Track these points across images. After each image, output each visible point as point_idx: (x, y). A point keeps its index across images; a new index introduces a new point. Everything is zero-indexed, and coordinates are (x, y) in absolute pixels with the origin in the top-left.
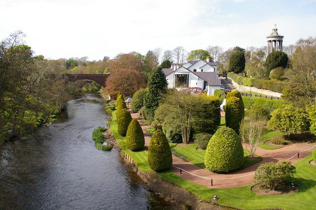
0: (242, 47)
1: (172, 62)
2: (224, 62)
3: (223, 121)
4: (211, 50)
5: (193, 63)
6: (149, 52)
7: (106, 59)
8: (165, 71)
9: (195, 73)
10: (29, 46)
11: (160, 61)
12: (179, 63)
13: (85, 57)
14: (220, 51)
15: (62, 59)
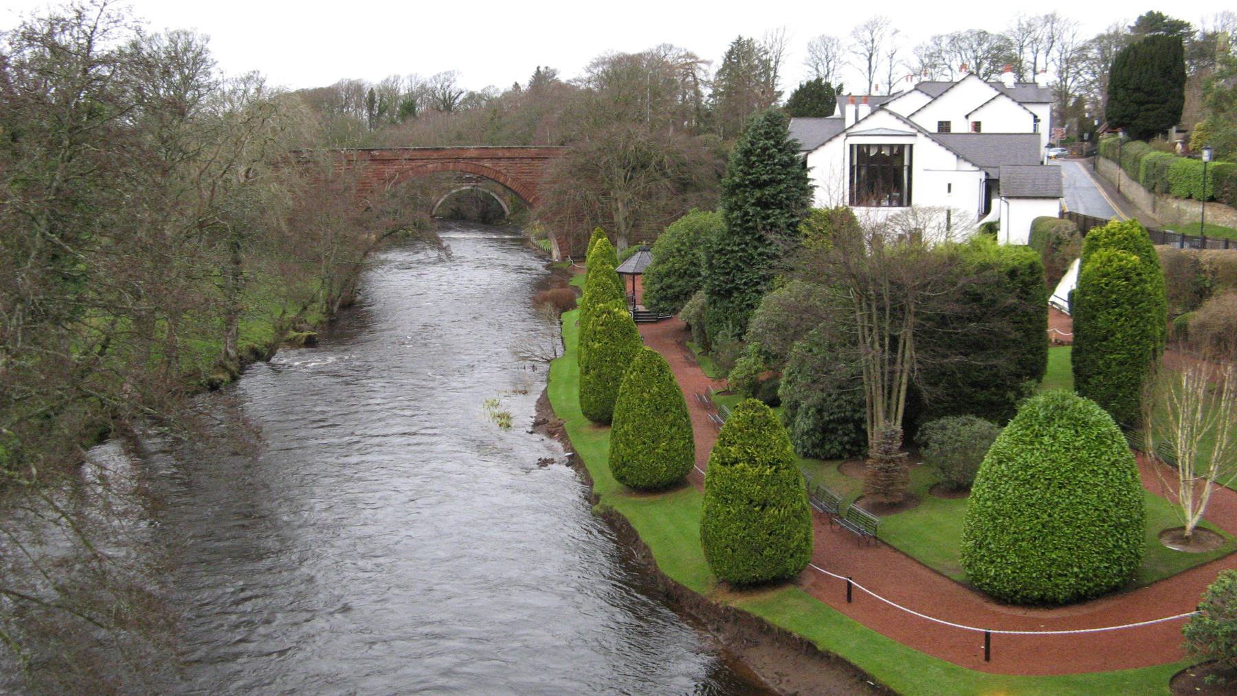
0: (1173, 13)
1: (840, 88)
2: (1087, 88)
3: (1059, 359)
4: (1027, 30)
5: (935, 90)
6: (739, 42)
7: (542, 80)
8: (799, 129)
9: (943, 137)
10: (1186, 22)
11: (788, 82)
12: (874, 93)
13: (452, 74)
14: (1067, 37)
15: (351, 83)
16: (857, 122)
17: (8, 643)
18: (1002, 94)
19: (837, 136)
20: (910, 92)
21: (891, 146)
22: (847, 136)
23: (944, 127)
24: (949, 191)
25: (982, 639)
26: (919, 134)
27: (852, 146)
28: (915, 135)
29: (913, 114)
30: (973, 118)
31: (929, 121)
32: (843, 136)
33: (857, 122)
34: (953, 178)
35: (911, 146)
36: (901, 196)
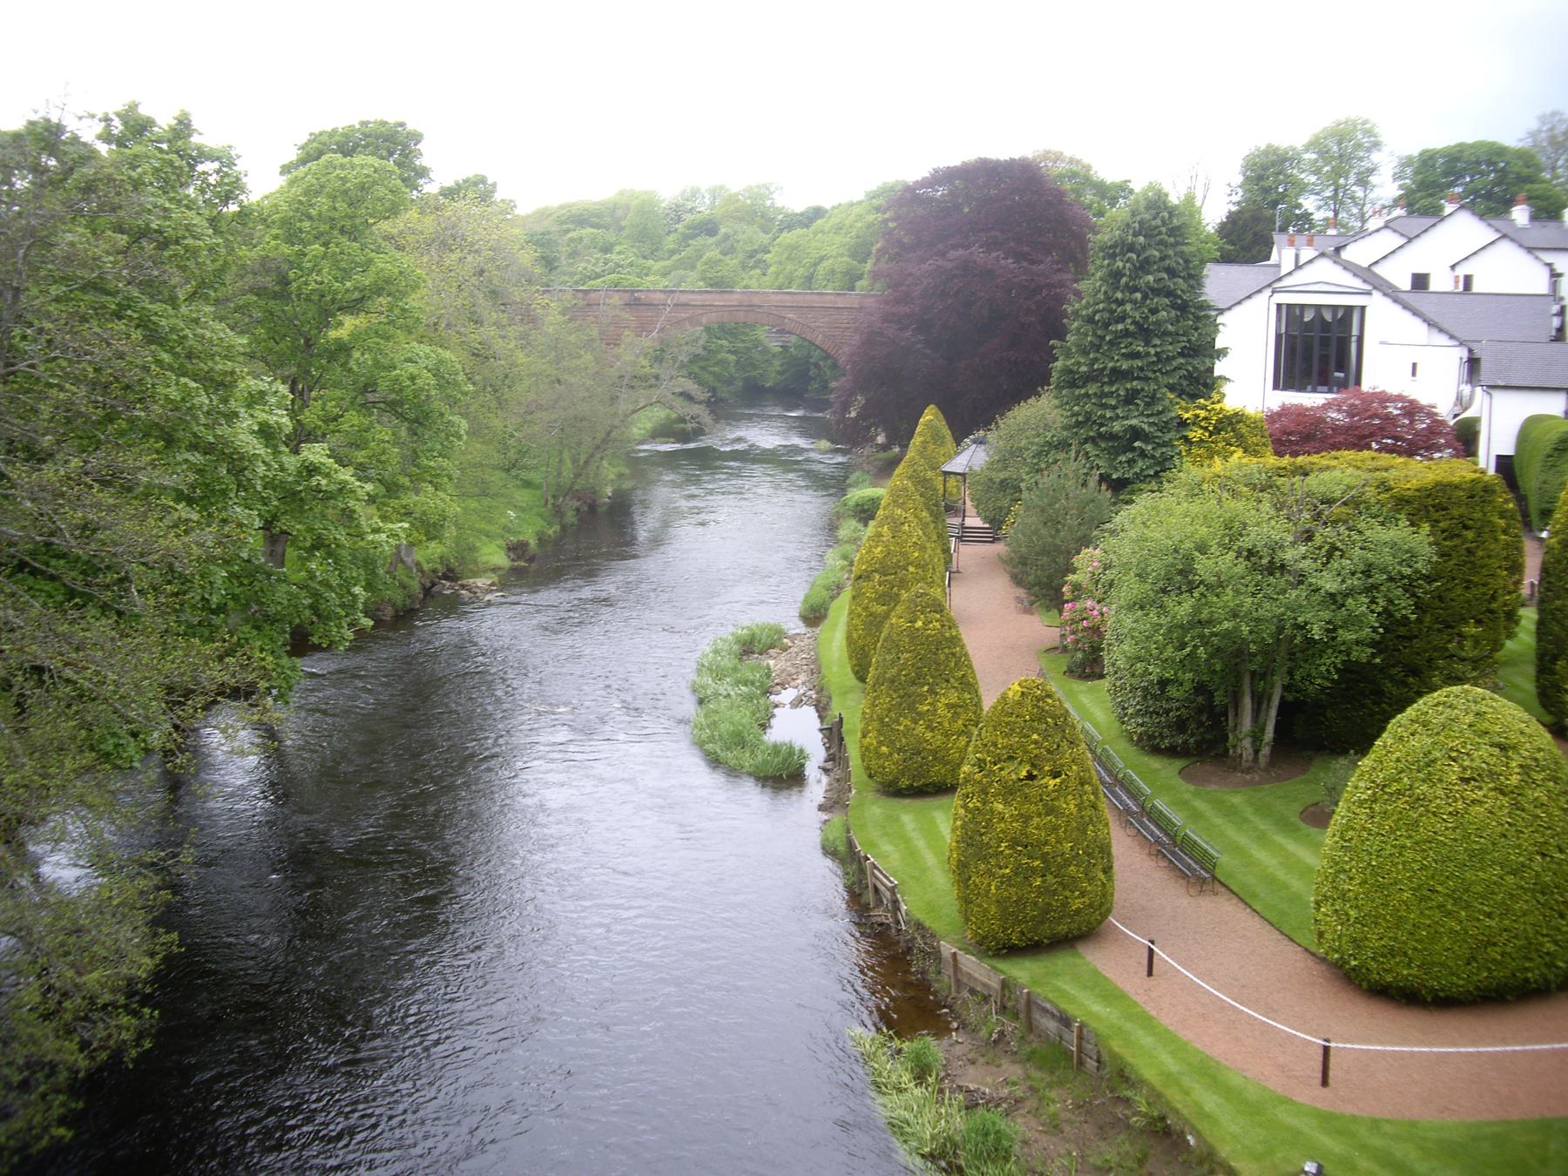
9: (1417, 299)
16: (1298, 267)
17: (223, 852)
18: (1504, 236)
19: (1259, 291)
20: (1378, 231)
21: (1334, 308)
22: (1273, 292)
23: (1420, 282)
24: (1414, 374)
25: (1321, 1051)
26: (1374, 292)
27: (1279, 306)
28: (1369, 293)
29: (1376, 262)
30: (1461, 271)
31: (1398, 274)
32: (1268, 292)
33: (1298, 267)
34: (1422, 357)
35: (1363, 308)
36: (1346, 379)
